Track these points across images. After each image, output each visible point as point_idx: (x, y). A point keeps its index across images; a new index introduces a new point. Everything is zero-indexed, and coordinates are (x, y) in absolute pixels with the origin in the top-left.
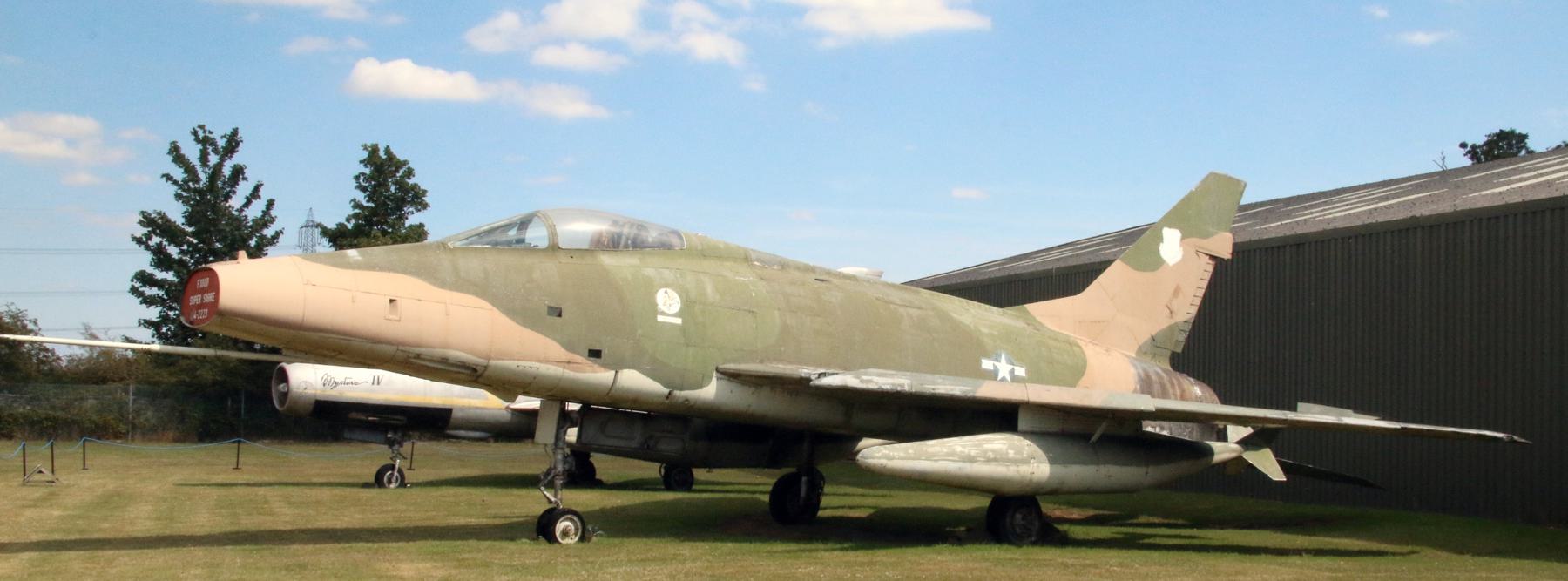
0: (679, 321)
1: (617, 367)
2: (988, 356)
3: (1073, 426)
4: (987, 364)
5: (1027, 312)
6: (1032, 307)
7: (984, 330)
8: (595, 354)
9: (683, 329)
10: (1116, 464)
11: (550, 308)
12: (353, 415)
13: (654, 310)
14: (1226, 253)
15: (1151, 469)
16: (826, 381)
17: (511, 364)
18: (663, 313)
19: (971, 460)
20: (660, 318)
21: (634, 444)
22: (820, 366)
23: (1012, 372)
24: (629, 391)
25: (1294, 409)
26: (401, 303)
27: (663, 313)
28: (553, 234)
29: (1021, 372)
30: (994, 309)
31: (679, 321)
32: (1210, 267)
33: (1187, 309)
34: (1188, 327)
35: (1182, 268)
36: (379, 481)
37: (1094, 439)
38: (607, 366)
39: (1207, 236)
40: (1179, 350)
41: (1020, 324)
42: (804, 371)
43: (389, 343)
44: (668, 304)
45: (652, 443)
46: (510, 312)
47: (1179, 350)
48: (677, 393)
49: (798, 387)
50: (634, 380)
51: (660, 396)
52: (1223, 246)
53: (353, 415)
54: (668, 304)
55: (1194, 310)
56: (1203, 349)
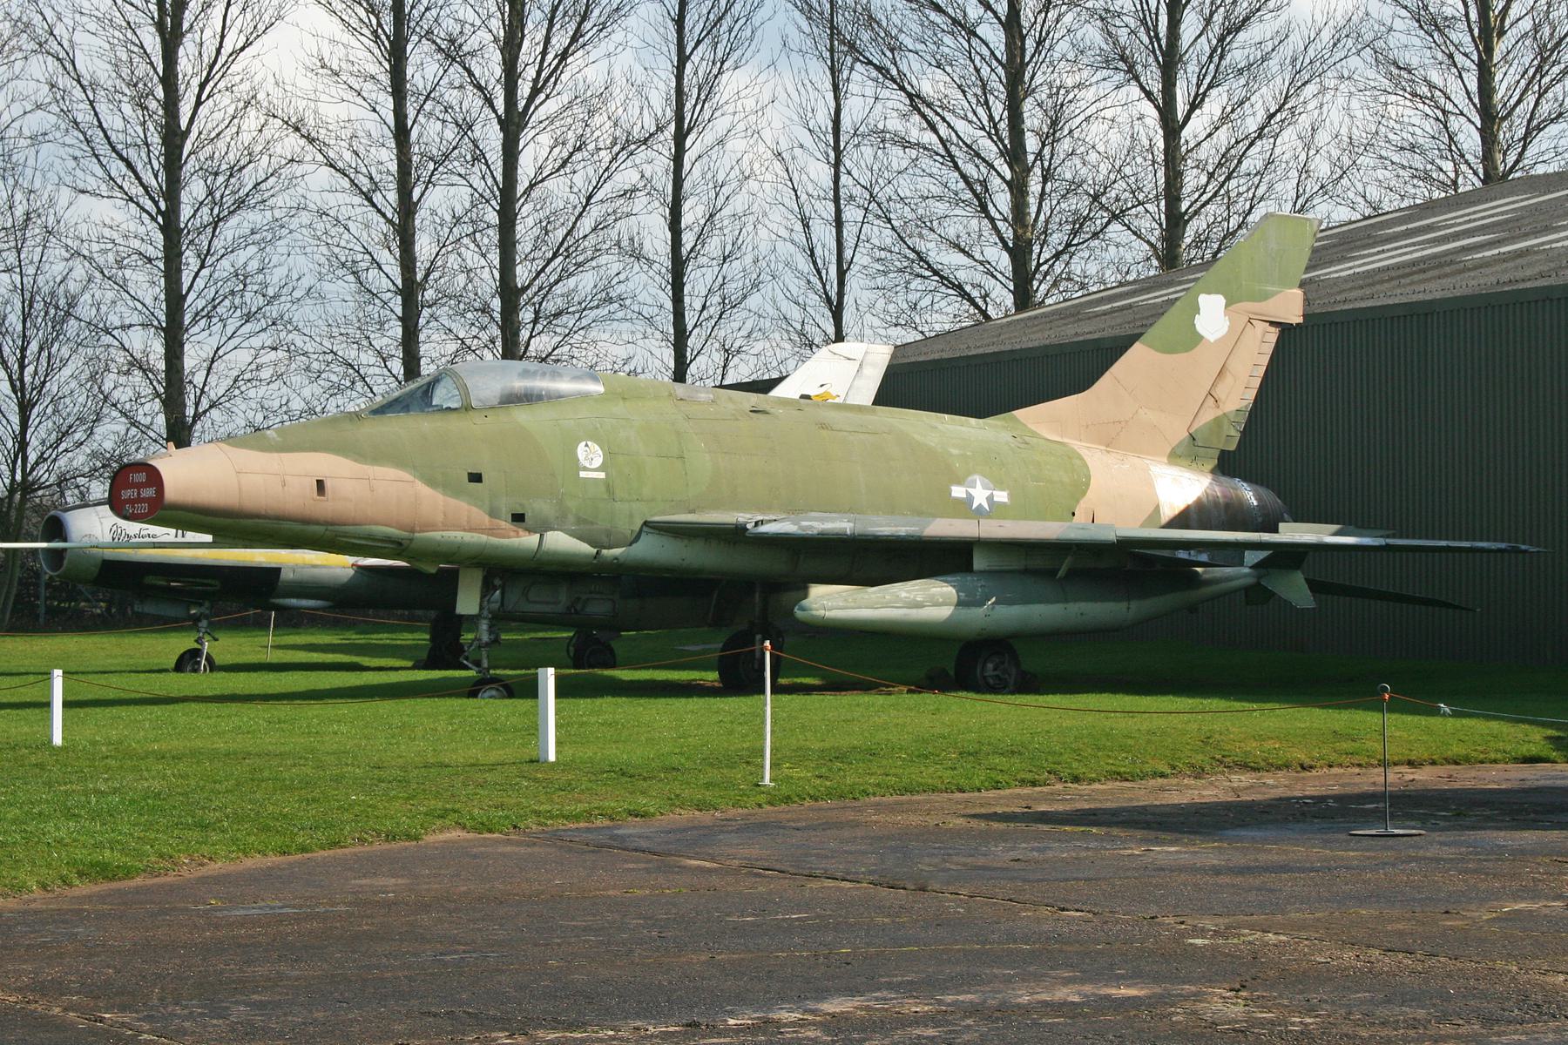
0: (602, 475)
1: (542, 528)
2: (959, 483)
3: (1038, 562)
4: (958, 492)
5: (1015, 419)
6: (1017, 413)
7: (955, 451)
8: (518, 518)
9: (608, 485)
10: (1086, 600)
11: (470, 474)
12: (150, 580)
13: (577, 466)
14: (1295, 317)
15: (1134, 605)
16: (763, 529)
17: (437, 535)
18: (585, 469)
19: (919, 605)
20: (583, 474)
21: (560, 608)
22: (760, 510)
23: (990, 499)
24: (555, 553)
25: (1276, 531)
26: (328, 484)
27: (585, 469)
28: (464, 391)
29: (1002, 496)
30: (973, 421)
31: (602, 475)
32: (1273, 335)
33: (1240, 393)
34: (1243, 419)
35: (1225, 341)
36: (179, 667)
37: (1061, 573)
38: (530, 531)
39: (1265, 297)
40: (1232, 447)
41: (1005, 436)
42: (745, 517)
43: (317, 523)
44: (590, 457)
45: (579, 607)
46: (431, 482)
47: (1232, 447)
48: (605, 552)
49: (735, 535)
50: (561, 542)
51: (587, 556)
52: (1290, 307)
53: (150, 580)
54: (590, 457)
55: (1251, 395)
56: (1267, 446)
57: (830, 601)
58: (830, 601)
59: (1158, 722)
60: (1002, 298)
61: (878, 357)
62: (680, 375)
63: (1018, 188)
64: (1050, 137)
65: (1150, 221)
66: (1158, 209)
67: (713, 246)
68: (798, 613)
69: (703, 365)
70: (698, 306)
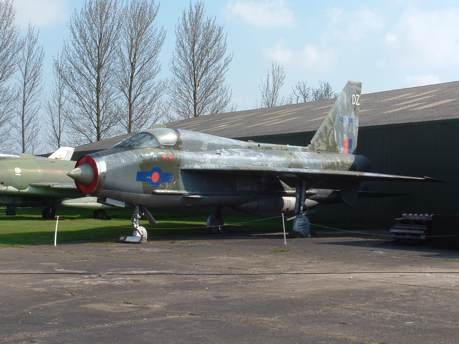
16: (55, 186)
20: (16, 174)
21: (10, 202)
31: (20, 175)
38: (5, 186)
50: (11, 189)
57: (69, 202)
58: (69, 202)
59: (336, 277)
60: (94, 138)
61: (71, 150)
62: (23, 152)
63: (98, 115)
64: (105, 104)
65: (125, 121)
66: (127, 119)
67: (31, 125)
68: (62, 203)
69: (29, 149)
70: (28, 137)
